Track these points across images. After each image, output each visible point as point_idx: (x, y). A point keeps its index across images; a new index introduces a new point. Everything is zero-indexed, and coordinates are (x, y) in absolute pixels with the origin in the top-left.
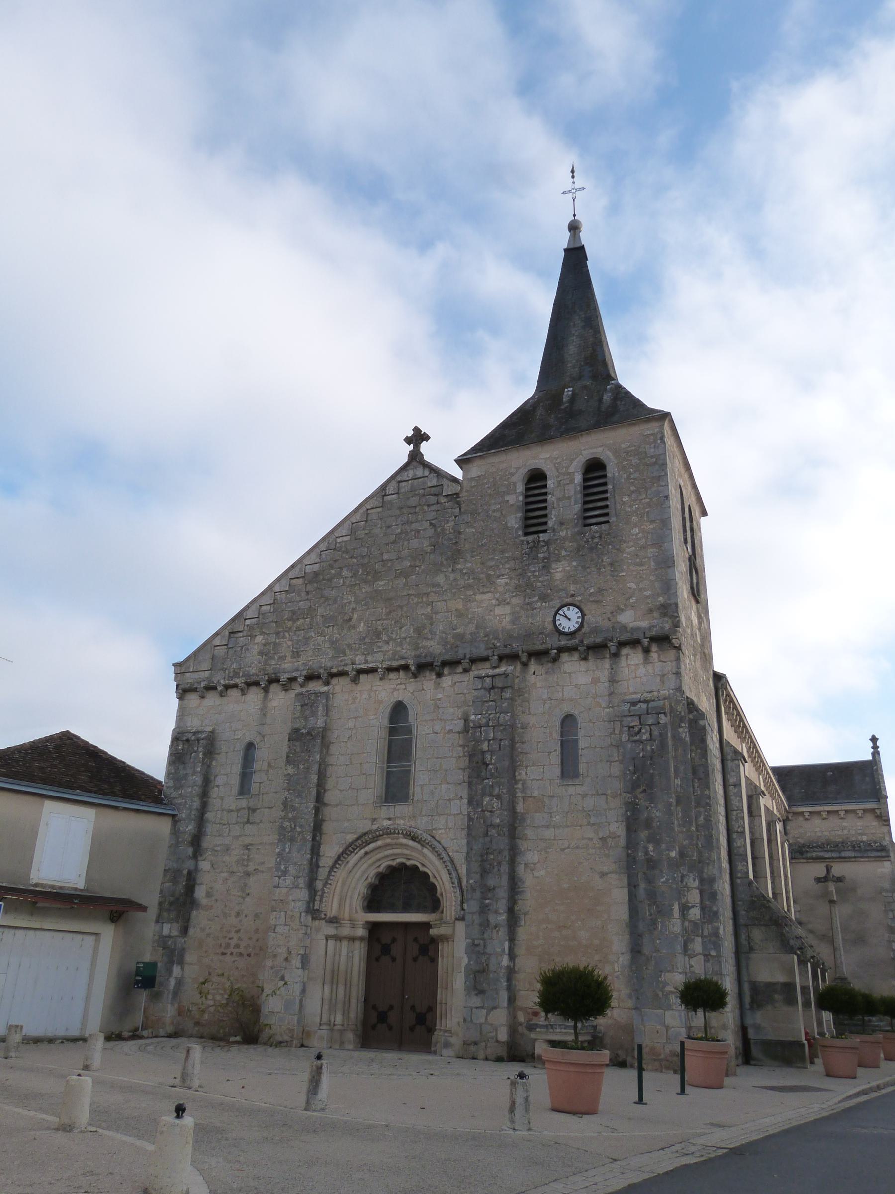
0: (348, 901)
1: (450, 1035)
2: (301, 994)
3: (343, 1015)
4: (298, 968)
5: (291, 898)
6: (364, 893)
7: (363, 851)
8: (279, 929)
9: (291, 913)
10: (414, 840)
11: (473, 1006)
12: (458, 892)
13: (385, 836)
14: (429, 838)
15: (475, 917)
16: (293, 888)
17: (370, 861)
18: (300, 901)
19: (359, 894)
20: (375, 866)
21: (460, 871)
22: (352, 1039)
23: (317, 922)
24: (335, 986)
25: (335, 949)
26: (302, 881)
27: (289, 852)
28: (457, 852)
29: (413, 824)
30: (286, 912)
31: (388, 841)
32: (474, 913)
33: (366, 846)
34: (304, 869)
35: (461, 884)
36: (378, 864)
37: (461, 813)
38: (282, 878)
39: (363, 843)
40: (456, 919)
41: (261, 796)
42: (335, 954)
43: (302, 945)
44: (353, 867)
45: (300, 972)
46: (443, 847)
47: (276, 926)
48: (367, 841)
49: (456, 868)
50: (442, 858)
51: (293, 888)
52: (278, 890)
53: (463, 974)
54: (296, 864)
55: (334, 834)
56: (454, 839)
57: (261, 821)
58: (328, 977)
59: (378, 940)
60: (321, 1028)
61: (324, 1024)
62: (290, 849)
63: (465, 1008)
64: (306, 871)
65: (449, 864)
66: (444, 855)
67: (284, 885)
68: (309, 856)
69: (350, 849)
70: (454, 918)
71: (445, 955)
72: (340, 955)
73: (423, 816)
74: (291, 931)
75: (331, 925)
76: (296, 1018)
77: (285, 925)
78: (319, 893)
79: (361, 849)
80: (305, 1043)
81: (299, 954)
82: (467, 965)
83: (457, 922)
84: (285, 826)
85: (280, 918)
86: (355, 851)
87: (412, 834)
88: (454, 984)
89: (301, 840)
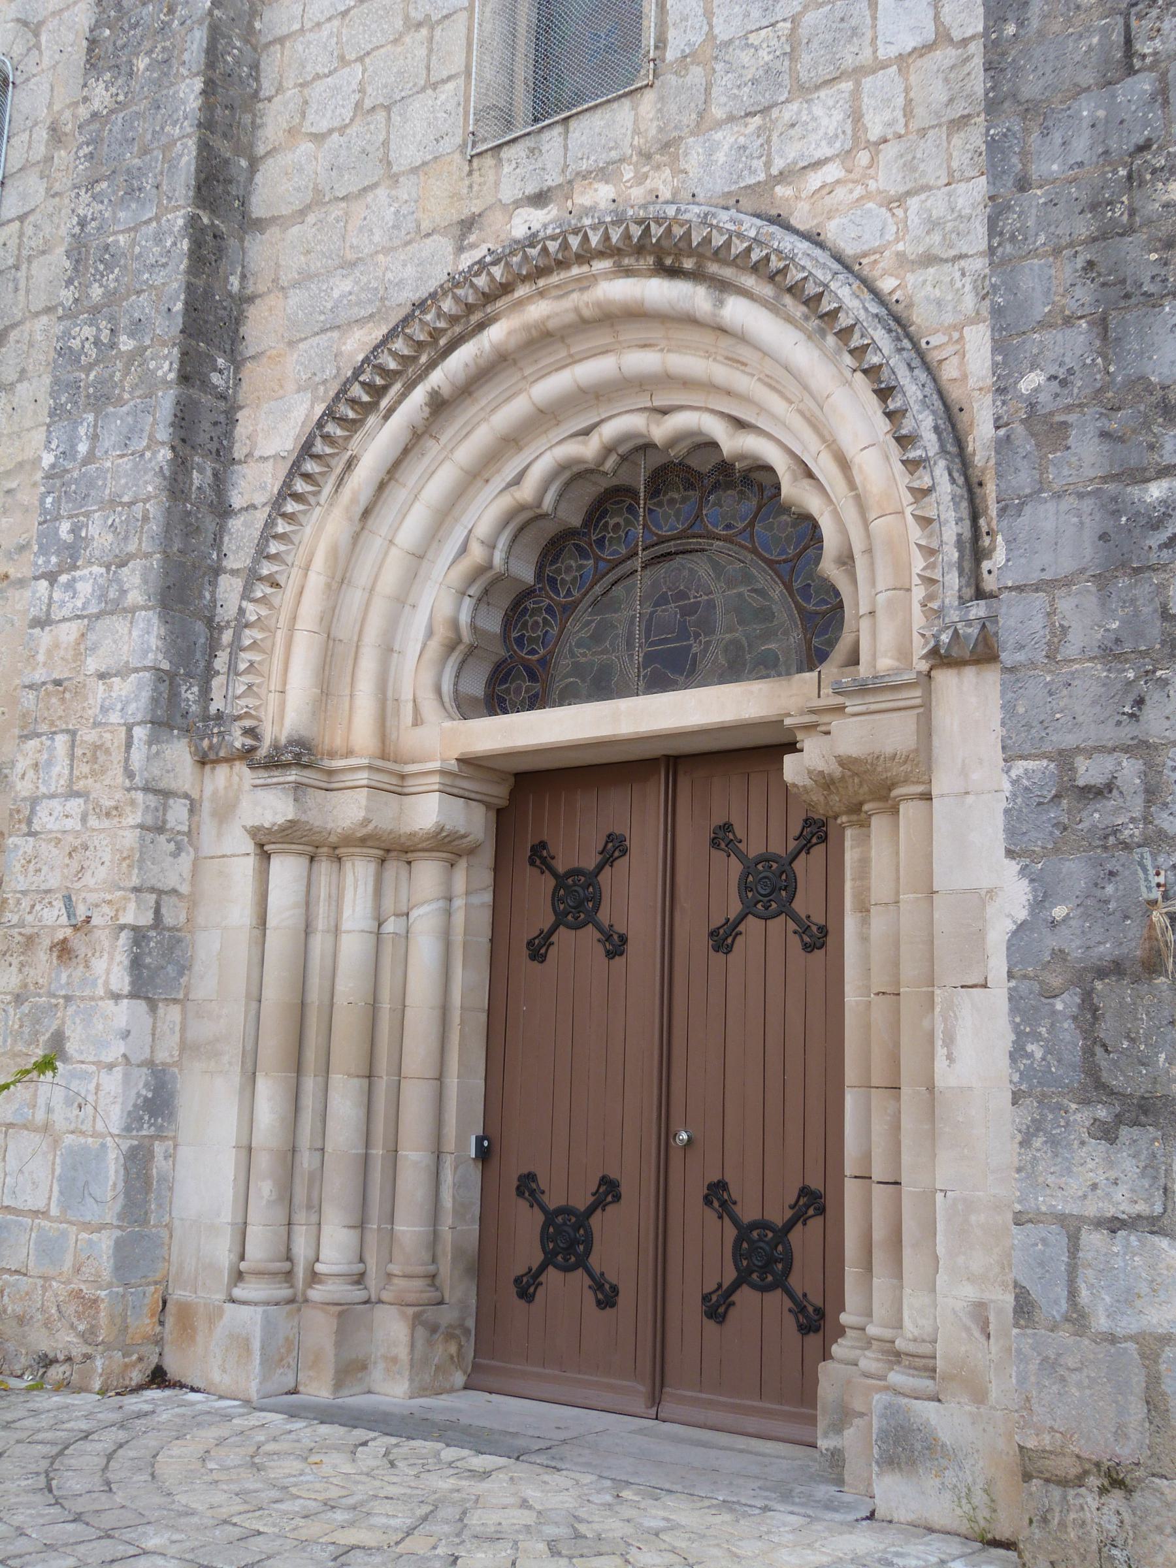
0: (368, 665)
1: (925, 1384)
2: (133, 1121)
3: (361, 1225)
4: (116, 997)
5: (92, 665)
6: (455, 624)
7: (419, 395)
8: (48, 818)
9: (88, 736)
10: (674, 272)
11: (1092, 1208)
12: (945, 488)
13: (522, 291)
14: (751, 227)
15: (1065, 605)
16: (98, 616)
17: (467, 452)
18: (124, 672)
19: (430, 633)
20: (498, 482)
21: (949, 372)
22: (403, 1352)
23: (220, 777)
24: (310, 1084)
25: (308, 903)
26: (137, 580)
27: (90, 458)
28: (929, 260)
29: (662, 183)
30: (73, 734)
31: (538, 311)
32: (1067, 582)
33: (432, 365)
34: (146, 518)
35: (960, 444)
36: (510, 470)
37: (943, 37)
38: (64, 578)
39: (420, 346)
40: (940, 658)
41: (22, 274)
42: (308, 930)
43: (135, 881)
44: (382, 487)
45: (123, 1013)
46: (838, 258)
47: (34, 801)
48: (435, 334)
49: (921, 355)
50: (833, 315)
51: (98, 616)
52: (45, 637)
53: (998, 996)
54: (113, 503)
55: (291, 344)
56: (900, 200)
57: (23, 371)
58: (272, 1044)
59: (540, 856)
60: (237, 1292)
61: (259, 1273)
62: (94, 438)
63: (1019, 1220)
64: (154, 527)
65: (880, 336)
66: (844, 293)
67: (66, 612)
68: (165, 454)
69: (356, 391)
70: (920, 648)
71: (880, 889)
72: (336, 931)
73: (719, 125)
74: (93, 822)
75: (278, 777)
76: (105, 1242)
77: (73, 794)
78: (227, 637)
79: (410, 387)
80: (173, 1369)
81: (122, 927)
82: (1022, 928)
83: (945, 679)
84: (75, 344)
85: (50, 763)
86: (384, 403)
87: (657, 231)
88: (940, 1063)
89: (134, 387)
